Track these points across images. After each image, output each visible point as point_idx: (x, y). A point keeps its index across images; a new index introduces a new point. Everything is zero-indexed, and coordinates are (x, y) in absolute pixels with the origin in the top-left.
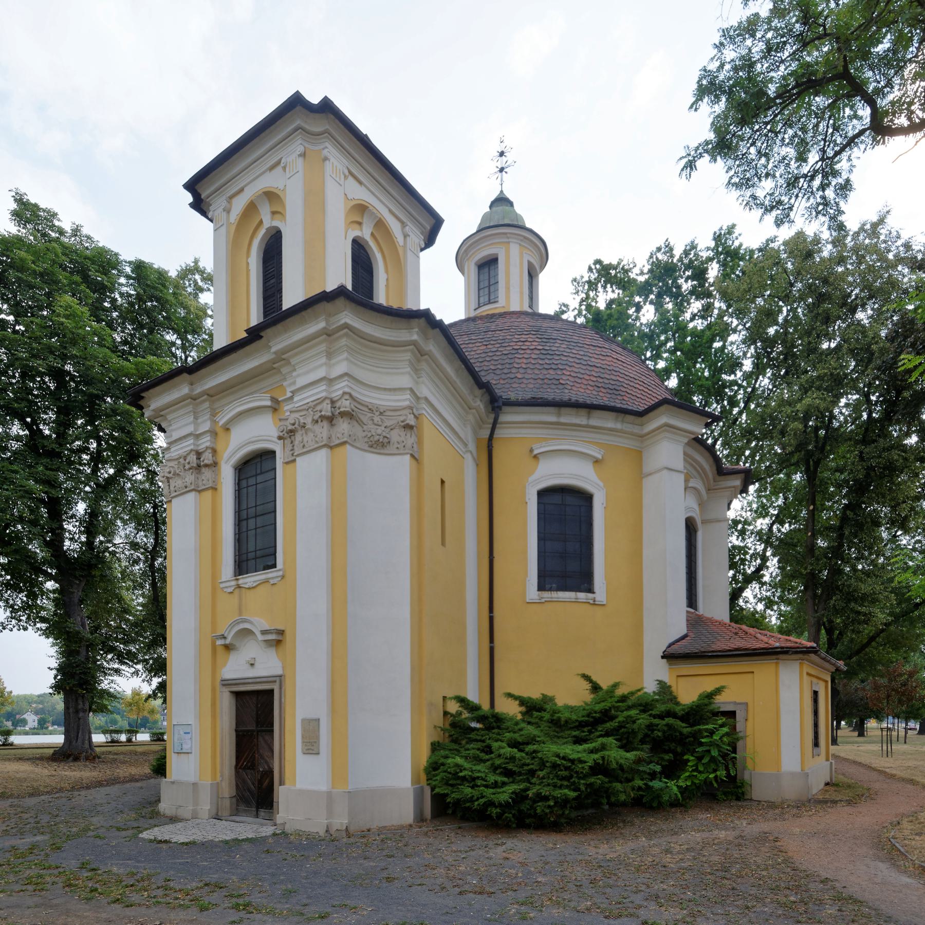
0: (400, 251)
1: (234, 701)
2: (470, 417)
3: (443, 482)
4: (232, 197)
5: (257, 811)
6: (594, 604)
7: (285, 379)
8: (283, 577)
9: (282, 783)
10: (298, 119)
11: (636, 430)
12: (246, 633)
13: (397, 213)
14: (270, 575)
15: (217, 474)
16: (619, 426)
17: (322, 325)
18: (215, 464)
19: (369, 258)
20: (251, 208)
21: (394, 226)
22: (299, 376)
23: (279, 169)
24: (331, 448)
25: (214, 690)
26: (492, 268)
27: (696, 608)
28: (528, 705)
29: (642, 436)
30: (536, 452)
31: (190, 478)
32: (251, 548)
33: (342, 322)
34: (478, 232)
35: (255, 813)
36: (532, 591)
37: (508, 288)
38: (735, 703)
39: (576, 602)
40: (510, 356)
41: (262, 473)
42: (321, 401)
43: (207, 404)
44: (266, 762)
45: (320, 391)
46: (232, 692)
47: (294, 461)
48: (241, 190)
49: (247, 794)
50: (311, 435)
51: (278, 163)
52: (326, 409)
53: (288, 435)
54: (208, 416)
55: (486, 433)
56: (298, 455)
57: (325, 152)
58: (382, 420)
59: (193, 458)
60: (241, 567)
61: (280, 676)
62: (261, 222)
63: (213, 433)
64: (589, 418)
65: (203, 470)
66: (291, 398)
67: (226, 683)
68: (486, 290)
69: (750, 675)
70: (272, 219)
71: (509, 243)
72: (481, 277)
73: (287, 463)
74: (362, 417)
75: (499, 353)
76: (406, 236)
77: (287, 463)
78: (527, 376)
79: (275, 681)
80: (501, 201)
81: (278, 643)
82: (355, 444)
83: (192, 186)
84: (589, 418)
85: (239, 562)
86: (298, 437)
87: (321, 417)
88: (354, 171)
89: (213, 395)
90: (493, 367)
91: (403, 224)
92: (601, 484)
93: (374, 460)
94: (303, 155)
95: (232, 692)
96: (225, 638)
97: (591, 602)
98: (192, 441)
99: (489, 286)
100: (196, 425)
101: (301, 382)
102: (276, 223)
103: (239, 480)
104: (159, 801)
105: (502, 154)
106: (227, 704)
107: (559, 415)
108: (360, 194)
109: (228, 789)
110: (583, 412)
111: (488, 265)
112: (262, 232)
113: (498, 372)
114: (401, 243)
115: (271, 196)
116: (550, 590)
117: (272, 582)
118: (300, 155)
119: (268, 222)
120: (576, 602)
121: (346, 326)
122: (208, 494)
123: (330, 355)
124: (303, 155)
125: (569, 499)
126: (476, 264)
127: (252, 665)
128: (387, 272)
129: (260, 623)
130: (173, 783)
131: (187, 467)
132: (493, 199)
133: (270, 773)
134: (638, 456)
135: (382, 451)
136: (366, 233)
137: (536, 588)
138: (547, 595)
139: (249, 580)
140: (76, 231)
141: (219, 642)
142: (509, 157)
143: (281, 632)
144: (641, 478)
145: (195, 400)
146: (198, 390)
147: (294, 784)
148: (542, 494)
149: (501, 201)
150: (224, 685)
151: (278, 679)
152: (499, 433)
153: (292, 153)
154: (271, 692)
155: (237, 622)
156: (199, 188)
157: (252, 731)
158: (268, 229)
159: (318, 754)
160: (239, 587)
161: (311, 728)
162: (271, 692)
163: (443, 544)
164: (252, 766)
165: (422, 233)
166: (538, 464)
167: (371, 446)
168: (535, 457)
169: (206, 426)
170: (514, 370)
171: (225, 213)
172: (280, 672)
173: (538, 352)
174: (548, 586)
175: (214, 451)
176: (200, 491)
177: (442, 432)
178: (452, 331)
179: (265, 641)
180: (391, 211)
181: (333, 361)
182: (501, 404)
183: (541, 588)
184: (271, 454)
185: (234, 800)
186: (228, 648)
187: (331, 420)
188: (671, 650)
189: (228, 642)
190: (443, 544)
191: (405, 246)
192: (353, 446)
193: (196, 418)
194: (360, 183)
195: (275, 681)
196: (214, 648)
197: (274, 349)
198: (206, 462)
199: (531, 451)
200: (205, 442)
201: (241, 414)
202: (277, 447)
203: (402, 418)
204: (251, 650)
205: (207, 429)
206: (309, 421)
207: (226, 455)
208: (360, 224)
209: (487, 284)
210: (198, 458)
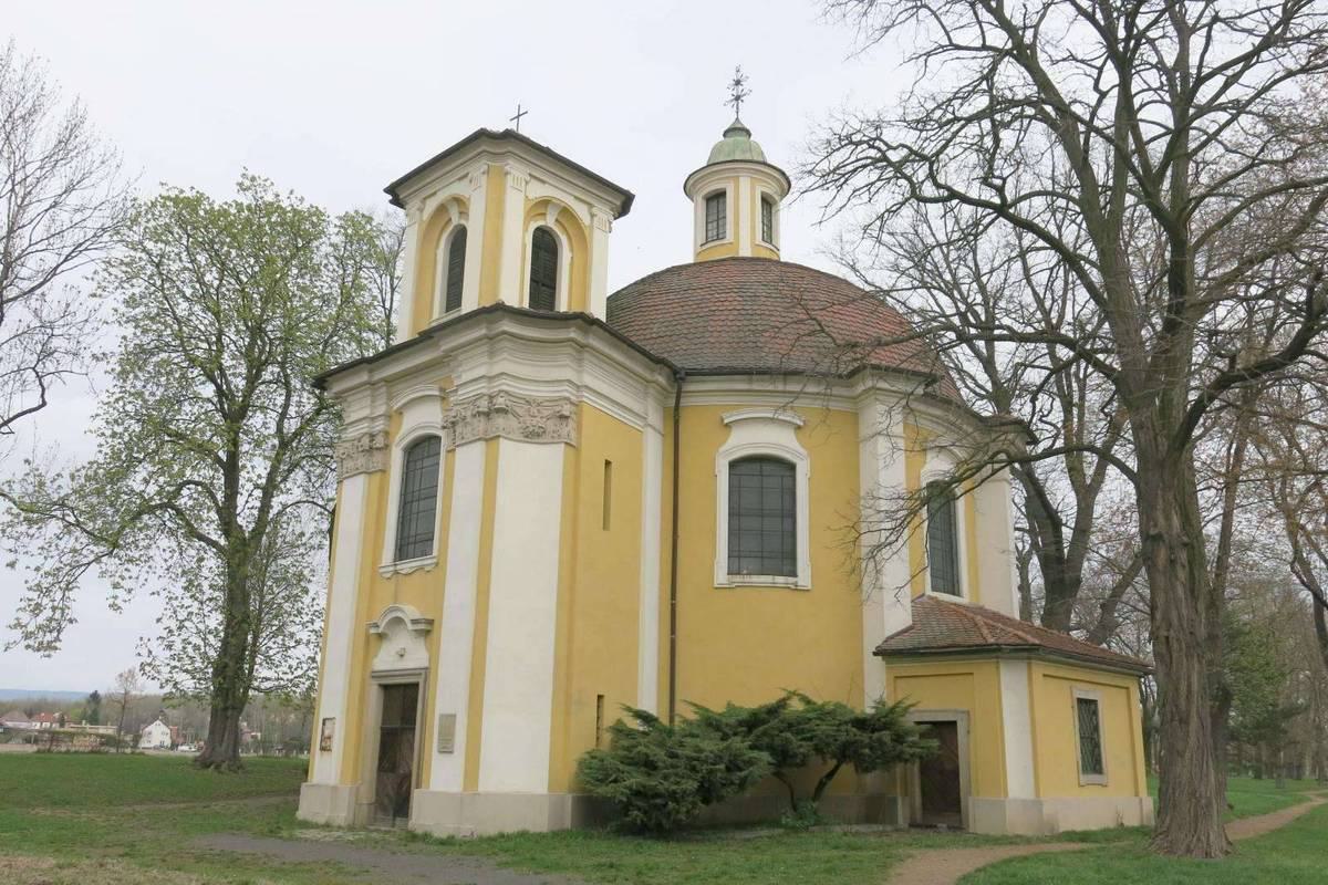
0: (587, 232)
2: (651, 391)
3: (608, 463)
4: (425, 199)
5: (394, 820)
6: (796, 589)
7: (452, 371)
8: (437, 564)
9: (418, 786)
12: (398, 621)
13: (583, 197)
14: (426, 562)
15: (389, 456)
17: (484, 331)
18: (387, 447)
19: (555, 242)
20: (442, 209)
21: (581, 211)
22: (465, 371)
23: (466, 181)
24: (486, 440)
25: (363, 680)
26: (721, 201)
27: (954, 589)
29: (854, 398)
30: (726, 421)
31: (361, 461)
32: (413, 533)
33: (501, 329)
34: (708, 166)
35: (391, 822)
36: (721, 576)
37: (737, 224)
38: (956, 712)
39: (774, 587)
40: (705, 319)
41: (428, 457)
42: (481, 396)
43: (384, 389)
44: (407, 763)
45: (482, 388)
46: (380, 685)
47: (454, 450)
48: (434, 194)
49: (386, 801)
50: (469, 428)
51: (466, 176)
52: (484, 405)
53: (451, 425)
54: (385, 400)
55: (672, 402)
56: (458, 446)
57: (507, 168)
58: (538, 411)
59: (366, 440)
60: (402, 553)
61: (426, 668)
62: (450, 219)
63: (388, 416)
64: (785, 384)
65: (375, 452)
66: (456, 391)
67: (376, 675)
68: (715, 224)
69: (970, 677)
70: (460, 218)
71: (738, 177)
72: (711, 210)
73: (449, 451)
74: (518, 410)
75: (694, 316)
76: (592, 216)
77: (449, 451)
79: (420, 674)
80: (737, 130)
81: (428, 632)
82: (510, 436)
83: (391, 190)
84: (785, 384)
85: (401, 545)
86: (459, 429)
87: (478, 412)
88: (534, 174)
89: (390, 381)
90: (685, 331)
91: (590, 205)
93: (531, 450)
94: (487, 172)
95: (380, 685)
96: (378, 626)
97: (793, 587)
98: (366, 425)
99: (718, 220)
100: (373, 407)
101: (465, 377)
102: (463, 222)
103: (408, 462)
104: (297, 809)
105: (738, 83)
106: (374, 697)
108: (538, 191)
109: (367, 793)
111: (716, 198)
112: (450, 228)
113: (690, 336)
115: (458, 200)
117: (427, 569)
118: (484, 173)
119: (456, 220)
121: (505, 333)
122: (377, 477)
123: (492, 354)
124: (487, 172)
125: (767, 468)
127: (402, 656)
128: (572, 250)
129: (410, 611)
130: (313, 786)
131: (360, 449)
132: (726, 128)
133: (408, 776)
134: (855, 417)
135: (540, 440)
136: (550, 221)
137: (726, 571)
138: (738, 579)
139: (407, 566)
141: (373, 631)
142: (746, 85)
143: (431, 622)
144: (858, 443)
145: (373, 384)
147: (428, 787)
148: (733, 465)
149: (737, 130)
150: (373, 677)
151: (423, 672)
152: (684, 402)
153: (478, 169)
154: (416, 685)
155: (392, 610)
156: (398, 191)
157: (396, 729)
158: (456, 226)
159: (451, 752)
160: (396, 572)
161: (449, 721)
162: (416, 685)
163: (606, 526)
164: (393, 768)
165: (612, 210)
166: (729, 435)
167: (527, 437)
168: (727, 425)
169: (382, 410)
170: (707, 334)
171: (418, 213)
172: (426, 664)
173: (736, 313)
175: (387, 433)
176: (369, 473)
177: (609, 412)
179: (416, 631)
180: (576, 198)
181: (495, 360)
182: (683, 375)
184: (438, 438)
185: (372, 807)
186: (381, 637)
187: (487, 415)
188: (885, 647)
189: (380, 630)
190: (606, 526)
191: (591, 227)
192: (506, 438)
193: (373, 402)
194: (543, 182)
195: (420, 674)
196: (368, 638)
197: (443, 348)
198: (378, 445)
199: (722, 420)
200: (380, 425)
201: (405, 405)
203: (558, 409)
204: (403, 640)
205: (382, 413)
206: (469, 413)
207: (397, 438)
208: (544, 214)
210: (372, 441)
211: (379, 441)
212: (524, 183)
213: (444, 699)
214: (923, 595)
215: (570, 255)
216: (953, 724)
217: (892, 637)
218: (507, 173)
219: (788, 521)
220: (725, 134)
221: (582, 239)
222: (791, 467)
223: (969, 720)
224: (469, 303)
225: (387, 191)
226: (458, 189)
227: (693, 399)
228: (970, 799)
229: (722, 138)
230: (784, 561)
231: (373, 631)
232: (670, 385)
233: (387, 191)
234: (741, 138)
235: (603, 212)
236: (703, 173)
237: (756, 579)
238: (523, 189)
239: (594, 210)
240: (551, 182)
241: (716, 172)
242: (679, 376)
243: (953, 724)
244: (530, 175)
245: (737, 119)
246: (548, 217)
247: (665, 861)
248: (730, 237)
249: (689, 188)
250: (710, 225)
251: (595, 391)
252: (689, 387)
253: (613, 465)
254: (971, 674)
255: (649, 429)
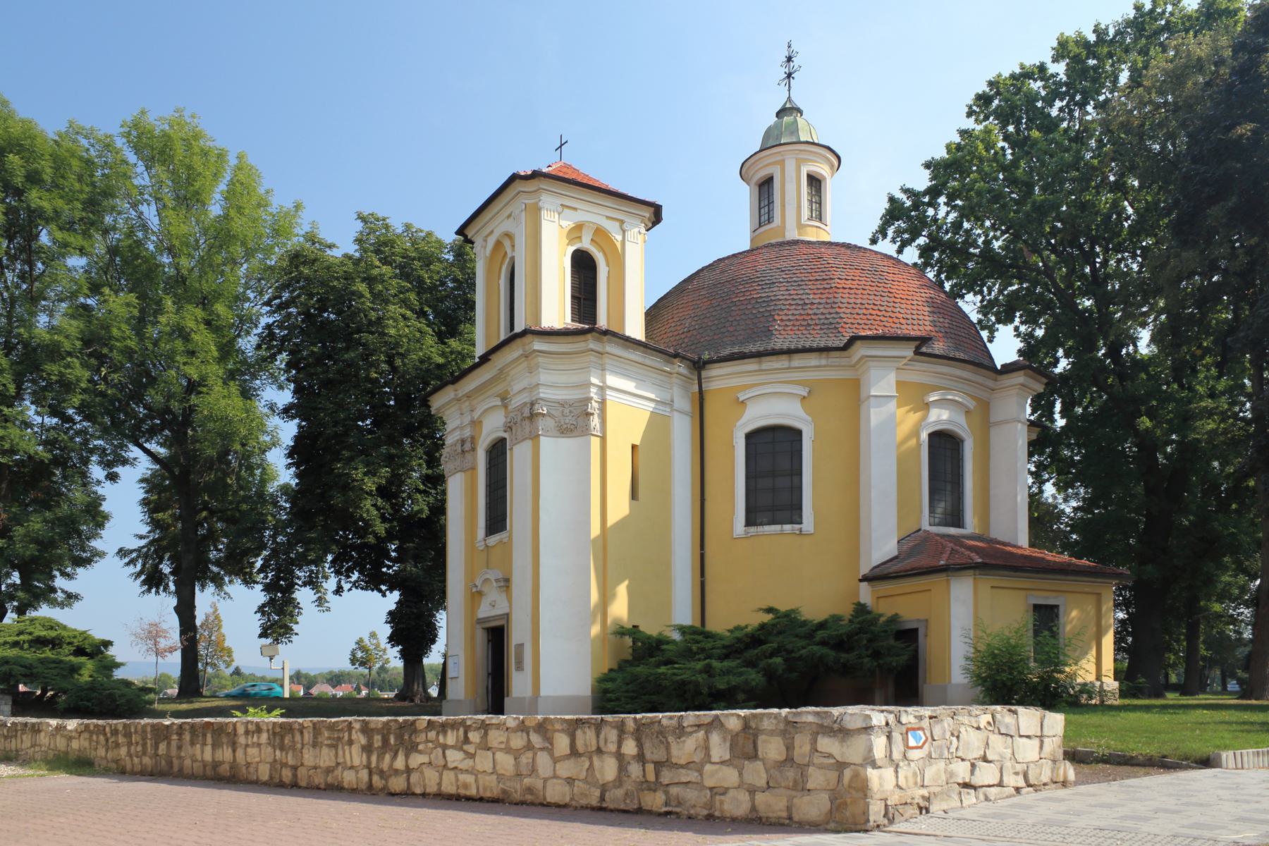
1: (485, 635)
2: (674, 380)
10: (518, 186)
11: (844, 361)
16: (823, 362)
17: (520, 352)
18: (473, 449)
20: (499, 244)
28: (832, 642)
30: (741, 399)
34: (761, 151)
37: (783, 206)
38: (918, 620)
43: (467, 403)
64: (790, 361)
67: (480, 621)
68: (766, 208)
78: (738, 328)
84: (790, 361)
89: (468, 396)
92: (810, 419)
105: (789, 59)
107: (760, 363)
110: (784, 357)
111: (765, 187)
114: (619, 238)
116: (762, 524)
120: (782, 533)
126: (756, 184)
128: (608, 265)
136: (586, 244)
137: (743, 523)
138: (753, 530)
140: (408, 227)
142: (796, 61)
146: (460, 394)
148: (749, 436)
161: (520, 646)
168: (742, 402)
170: (727, 325)
174: (759, 521)
178: (754, 247)
180: (608, 217)
183: (749, 522)
194: (575, 209)
196: (473, 594)
201: (486, 411)
202: (505, 435)
207: (480, 442)
208: (580, 237)
209: (766, 203)
211: (468, 446)
213: (517, 635)
214: (920, 530)
216: (916, 630)
217: (875, 567)
219: (795, 479)
222: (798, 433)
223: (927, 627)
224: (518, 329)
226: (507, 226)
227: (714, 383)
228: (925, 686)
230: (789, 510)
231: (474, 590)
232: (691, 373)
237: (767, 528)
242: (699, 366)
243: (916, 630)
247: (107, 638)
248: (777, 220)
249: (744, 172)
250: (762, 210)
252: (704, 374)
253: (136, 586)
255: (676, 414)
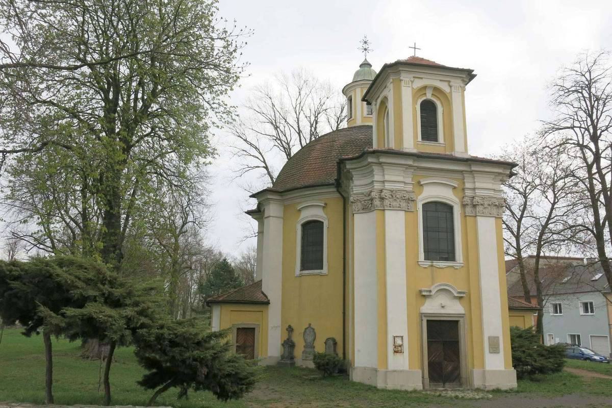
0: (449, 98)
21: (444, 87)
48: (379, 97)
69: (261, 313)
136: (429, 96)
148: (424, 205)
191: (451, 92)
194: (422, 78)
208: (425, 94)
212: (410, 83)
215: (442, 109)
218: (401, 80)
220: (361, 66)
221: (447, 99)
225: (475, 76)
229: (359, 68)
233: (475, 76)
234: (366, 69)
235: (456, 83)
236: (350, 86)
238: (410, 85)
239: (451, 84)
240: (425, 77)
241: (349, 88)
244: (414, 77)
245: (366, 59)
246: (427, 95)
251: (398, 182)
254: (262, 311)
